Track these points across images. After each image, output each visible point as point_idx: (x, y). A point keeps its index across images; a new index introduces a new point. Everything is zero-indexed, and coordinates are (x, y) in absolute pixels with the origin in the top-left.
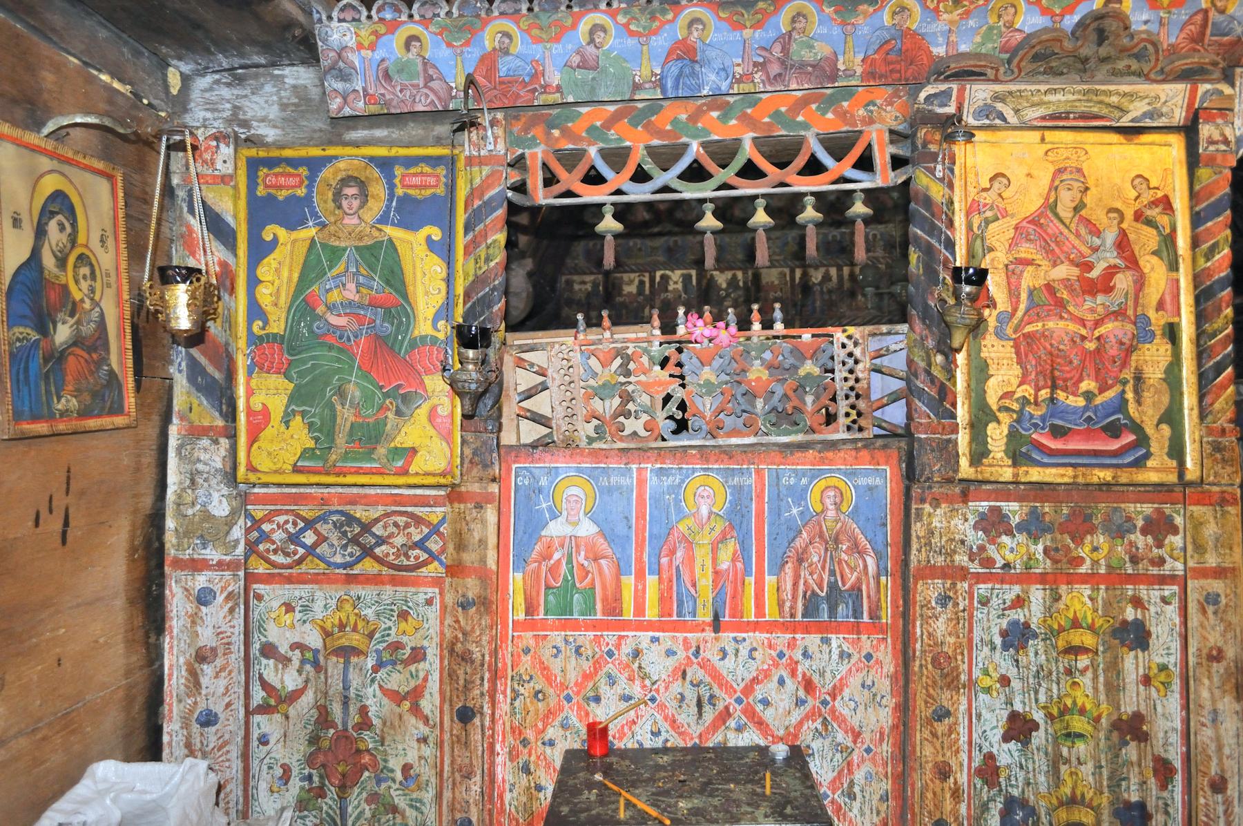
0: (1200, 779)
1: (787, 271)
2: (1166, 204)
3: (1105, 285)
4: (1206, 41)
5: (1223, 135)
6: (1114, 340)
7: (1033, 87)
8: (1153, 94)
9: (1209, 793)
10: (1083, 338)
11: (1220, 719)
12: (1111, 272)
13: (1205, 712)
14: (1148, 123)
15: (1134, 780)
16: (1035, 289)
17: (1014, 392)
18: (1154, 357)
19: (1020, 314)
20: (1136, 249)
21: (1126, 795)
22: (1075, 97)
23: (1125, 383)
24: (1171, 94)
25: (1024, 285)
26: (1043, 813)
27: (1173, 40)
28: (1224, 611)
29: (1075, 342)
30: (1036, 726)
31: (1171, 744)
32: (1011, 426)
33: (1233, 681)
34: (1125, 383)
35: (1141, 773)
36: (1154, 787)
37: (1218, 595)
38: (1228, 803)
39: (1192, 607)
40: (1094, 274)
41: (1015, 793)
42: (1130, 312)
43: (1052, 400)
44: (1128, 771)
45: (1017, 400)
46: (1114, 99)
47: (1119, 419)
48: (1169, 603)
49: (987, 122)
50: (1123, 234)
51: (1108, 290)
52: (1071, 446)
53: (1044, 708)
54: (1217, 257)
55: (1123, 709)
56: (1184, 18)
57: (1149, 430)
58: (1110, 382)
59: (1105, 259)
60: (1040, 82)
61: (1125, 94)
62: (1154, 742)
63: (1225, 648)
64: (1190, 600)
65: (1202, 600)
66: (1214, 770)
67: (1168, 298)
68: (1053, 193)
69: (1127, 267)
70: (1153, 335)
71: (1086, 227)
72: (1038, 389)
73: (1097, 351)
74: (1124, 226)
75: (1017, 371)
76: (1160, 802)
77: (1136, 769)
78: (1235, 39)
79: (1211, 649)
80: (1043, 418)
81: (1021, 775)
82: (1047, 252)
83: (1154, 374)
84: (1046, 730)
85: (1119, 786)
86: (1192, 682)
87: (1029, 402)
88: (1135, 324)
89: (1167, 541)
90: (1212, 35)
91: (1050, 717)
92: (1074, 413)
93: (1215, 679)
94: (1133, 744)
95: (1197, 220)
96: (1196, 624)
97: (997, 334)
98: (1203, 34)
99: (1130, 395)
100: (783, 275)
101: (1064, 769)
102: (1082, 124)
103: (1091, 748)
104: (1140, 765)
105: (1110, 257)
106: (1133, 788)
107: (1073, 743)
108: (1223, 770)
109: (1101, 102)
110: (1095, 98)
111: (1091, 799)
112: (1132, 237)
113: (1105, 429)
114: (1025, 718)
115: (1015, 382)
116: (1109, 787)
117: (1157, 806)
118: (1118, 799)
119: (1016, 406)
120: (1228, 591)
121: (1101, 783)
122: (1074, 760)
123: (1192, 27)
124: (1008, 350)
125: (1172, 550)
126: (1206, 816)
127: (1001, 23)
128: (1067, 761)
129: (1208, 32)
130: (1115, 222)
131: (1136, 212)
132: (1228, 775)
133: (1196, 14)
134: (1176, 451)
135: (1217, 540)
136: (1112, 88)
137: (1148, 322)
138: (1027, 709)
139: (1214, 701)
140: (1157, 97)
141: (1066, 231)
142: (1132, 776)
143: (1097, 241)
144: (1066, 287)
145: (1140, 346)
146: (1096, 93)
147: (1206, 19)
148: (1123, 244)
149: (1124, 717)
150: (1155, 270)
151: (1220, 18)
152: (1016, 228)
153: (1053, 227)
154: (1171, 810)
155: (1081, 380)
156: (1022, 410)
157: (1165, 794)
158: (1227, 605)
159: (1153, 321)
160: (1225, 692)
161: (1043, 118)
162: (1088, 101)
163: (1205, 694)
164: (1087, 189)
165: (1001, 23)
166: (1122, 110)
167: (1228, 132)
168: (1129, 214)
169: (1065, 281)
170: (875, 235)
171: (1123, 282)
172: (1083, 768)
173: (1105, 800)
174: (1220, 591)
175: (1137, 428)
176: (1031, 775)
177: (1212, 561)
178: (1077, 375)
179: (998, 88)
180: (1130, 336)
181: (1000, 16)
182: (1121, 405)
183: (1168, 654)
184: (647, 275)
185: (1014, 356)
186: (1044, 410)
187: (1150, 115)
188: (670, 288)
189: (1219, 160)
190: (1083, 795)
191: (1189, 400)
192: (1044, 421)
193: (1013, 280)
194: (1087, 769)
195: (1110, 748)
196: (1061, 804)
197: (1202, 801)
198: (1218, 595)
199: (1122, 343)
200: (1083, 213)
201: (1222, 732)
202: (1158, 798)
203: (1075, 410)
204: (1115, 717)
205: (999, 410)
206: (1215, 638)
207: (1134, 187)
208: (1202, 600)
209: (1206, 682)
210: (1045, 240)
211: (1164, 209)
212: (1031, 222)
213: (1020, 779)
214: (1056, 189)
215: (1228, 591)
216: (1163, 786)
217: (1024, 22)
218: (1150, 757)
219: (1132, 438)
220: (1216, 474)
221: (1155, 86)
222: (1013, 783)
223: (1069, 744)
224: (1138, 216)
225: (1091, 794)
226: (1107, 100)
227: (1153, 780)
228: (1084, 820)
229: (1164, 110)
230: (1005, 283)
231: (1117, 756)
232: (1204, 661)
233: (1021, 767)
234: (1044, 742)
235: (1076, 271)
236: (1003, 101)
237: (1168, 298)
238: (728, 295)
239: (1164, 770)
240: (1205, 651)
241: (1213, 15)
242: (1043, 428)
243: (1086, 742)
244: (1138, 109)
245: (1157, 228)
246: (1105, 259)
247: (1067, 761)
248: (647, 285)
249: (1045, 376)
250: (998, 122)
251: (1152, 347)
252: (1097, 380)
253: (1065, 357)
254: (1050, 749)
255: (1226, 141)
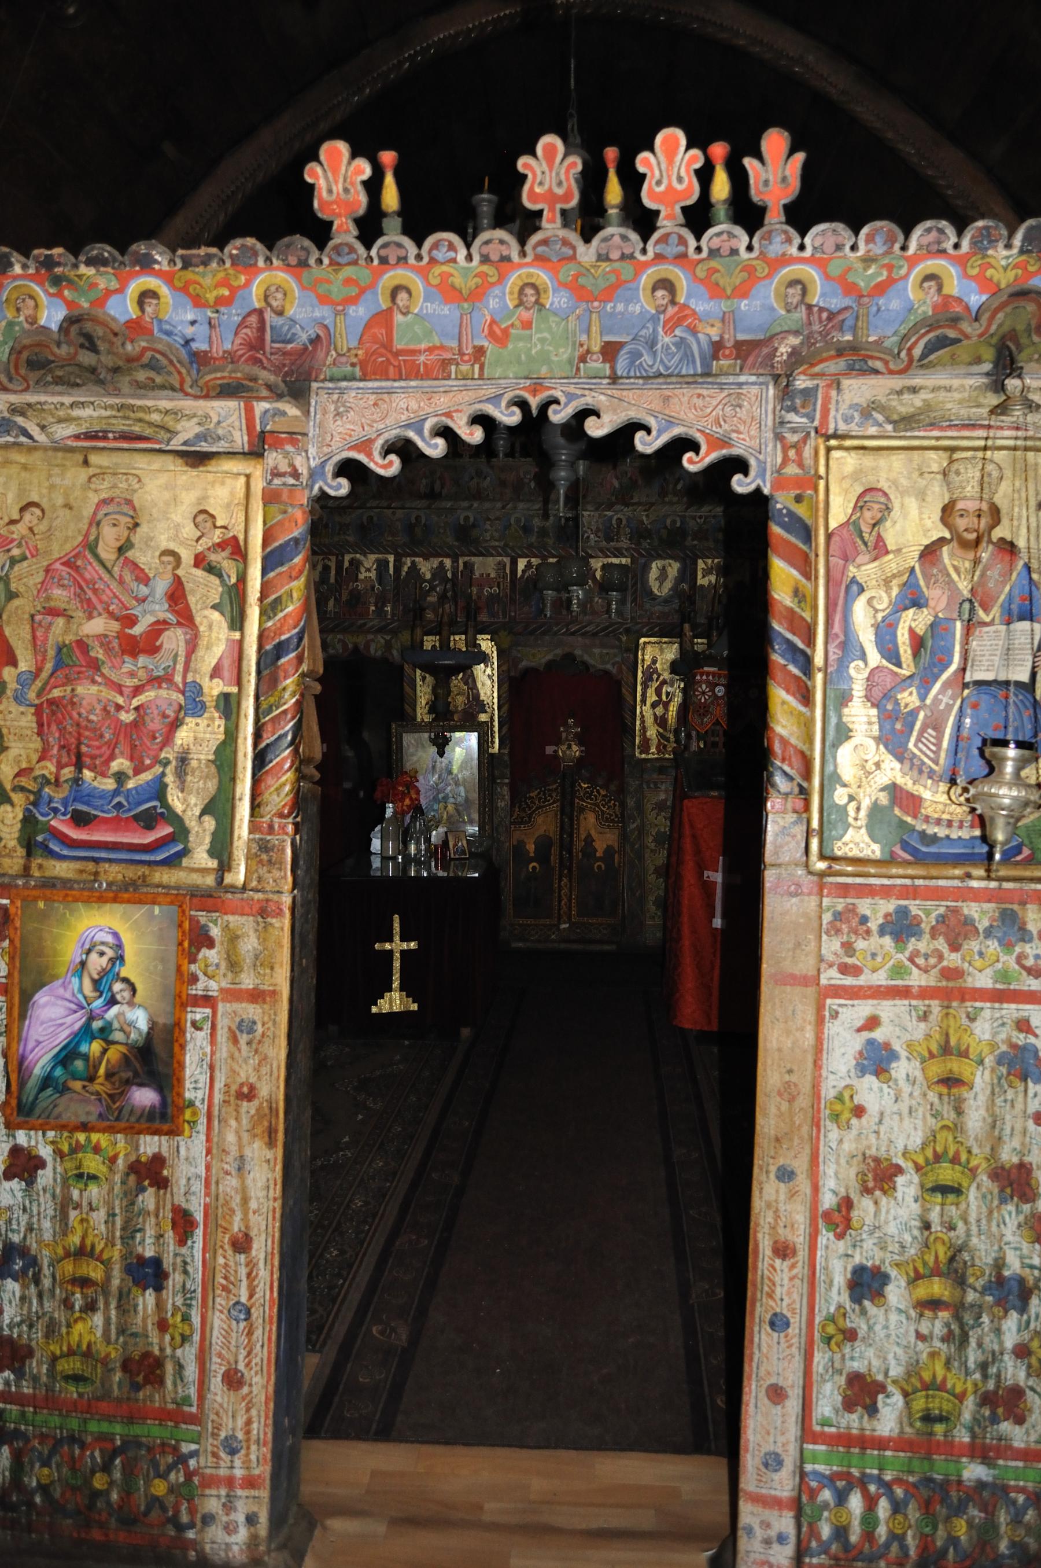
0: (220, 1235)
1: (507, 560)
2: (238, 550)
3: (148, 645)
4: (268, 349)
5: (292, 465)
6: (156, 712)
7: (56, 399)
8: (200, 413)
9: (230, 1252)
10: (119, 708)
11: (247, 1167)
12: (159, 628)
13: (230, 1159)
14: (204, 447)
15: (150, 1232)
16: (65, 646)
17: (31, 769)
18: (199, 735)
19: (44, 675)
20: (192, 600)
21: (140, 1249)
22: (108, 413)
23: (166, 763)
24: (223, 413)
25: (51, 641)
26: (46, 1263)
27: (228, 346)
28: (260, 1042)
29: (108, 712)
30: (41, 1164)
31: (194, 1193)
32: (27, 810)
33: (266, 1124)
34: (166, 763)
35: (158, 1224)
36: (172, 1242)
37: (254, 1023)
38: (251, 1265)
39: (222, 1035)
40: (137, 630)
41: (16, 1238)
42: (178, 679)
43: (77, 781)
44: (144, 1222)
45: (35, 779)
46: (155, 417)
47: (155, 807)
48: (200, 1029)
49: (11, 439)
50: (178, 582)
51: (153, 650)
52: (97, 837)
53: (52, 1143)
54: (281, 615)
55: (142, 1150)
56: (237, 319)
57: (191, 823)
58: (148, 762)
59: (152, 612)
60: (60, 394)
61: (167, 412)
62: (175, 1190)
63: (258, 1086)
64: (219, 1027)
65: (234, 1027)
66: (237, 1225)
67: (226, 663)
68: (94, 530)
69: (179, 624)
70: (203, 707)
71: (132, 572)
72: (60, 766)
73: (135, 724)
74: (180, 572)
75: (37, 744)
76: (179, 1260)
77: (153, 1220)
78: (300, 346)
79: (242, 1085)
80: (65, 802)
81: (24, 1219)
82: (81, 601)
83: (203, 755)
84: (55, 1169)
85: (133, 1238)
86: (216, 1123)
87: (48, 782)
88: (183, 693)
89: (200, 956)
90: (273, 341)
91: (59, 1153)
92: (101, 797)
93: (244, 1121)
94: (151, 1191)
95: (269, 563)
96: (225, 1055)
97: (16, 699)
98: (261, 339)
99: (170, 779)
100: (501, 566)
101: (73, 1214)
102: (125, 445)
103: (104, 1192)
104: (157, 1216)
105: (159, 610)
106: (148, 1241)
107: (86, 1185)
108: (247, 1227)
109: (140, 420)
110: (132, 415)
111: (102, 1251)
112: (188, 586)
113: (136, 818)
114: (29, 1153)
115: (35, 757)
116: (122, 1238)
117: (174, 1264)
118: (131, 1253)
119: (32, 786)
120: (266, 1019)
121: (113, 1233)
122: (85, 1204)
123: (247, 331)
124: (28, 721)
125: (206, 966)
126: (226, 1278)
127: (22, 318)
128: (78, 1206)
129: (268, 337)
130: (170, 567)
131: (197, 556)
132: (252, 1234)
133: (249, 314)
134: (221, 848)
135: (257, 957)
136: (149, 403)
137: (199, 689)
138: (33, 1143)
139: (241, 1147)
140: (207, 416)
141: (106, 576)
142: (147, 1227)
143: (144, 590)
144: (102, 645)
145: (188, 720)
146: (132, 408)
147: (262, 321)
148: (177, 595)
149: (143, 1159)
150: (215, 630)
151: (278, 321)
152: (47, 571)
153: (92, 571)
154: (190, 1269)
155: (112, 757)
156: (40, 790)
157: (184, 1250)
158: (263, 1035)
159: (206, 690)
160: (255, 1136)
161: (77, 437)
162: (125, 418)
163: (231, 1137)
164: (137, 525)
165: (22, 318)
166: (168, 431)
167: (299, 462)
168: (187, 556)
169: (103, 639)
170: (619, 520)
171: (174, 640)
172: (94, 1214)
173: (116, 1253)
174: (256, 1018)
175: (176, 820)
176: (35, 1220)
177: (248, 981)
178: (108, 753)
179: (13, 398)
180: (176, 707)
181: (18, 310)
182: (159, 790)
183: (195, 1088)
184: (333, 558)
185: (34, 725)
186: (66, 794)
187: (201, 437)
188: (361, 577)
189: (285, 496)
190: (93, 1246)
191: (244, 787)
192: (65, 804)
193: (39, 633)
194: (99, 1217)
195: (125, 1194)
196: (68, 1254)
197: (221, 1261)
198: (254, 1023)
199: (164, 716)
200: (130, 554)
201: (249, 1182)
202: (176, 1255)
203: (103, 794)
204: (133, 1158)
205: (14, 789)
206: (246, 1073)
207: (196, 526)
208: (234, 1027)
209: (233, 1123)
210: (81, 587)
211: (232, 554)
212: (67, 564)
213: (23, 1224)
214: (98, 524)
215: (266, 1019)
216: (182, 1242)
217: (49, 317)
218: (169, 1207)
219: (169, 830)
220: (260, 880)
221: (201, 403)
222: (15, 1227)
223: (81, 1186)
224: (199, 561)
225: (102, 1244)
226: (147, 417)
227: (171, 1233)
228: (92, 1275)
229: (220, 432)
230: (29, 637)
231: (133, 1204)
232: (232, 1099)
233: (25, 1210)
234: (51, 1182)
235: (115, 626)
236: (23, 414)
237: (226, 663)
238: (433, 588)
239: (183, 1223)
240: (234, 1088)
241: (268, 315)
242: (64, 814)
243: (99, 1186)
244: (187, 431)
245: (220, 576)
246: (152, 612)
247: (78, 1206)
248: (333, 572)
249: (69, 751)
250: (23, 439)
251: (203, 722)
252: (132, 759)
253: (94, 730)
254: (58, 1191)
255: (295, 474)
